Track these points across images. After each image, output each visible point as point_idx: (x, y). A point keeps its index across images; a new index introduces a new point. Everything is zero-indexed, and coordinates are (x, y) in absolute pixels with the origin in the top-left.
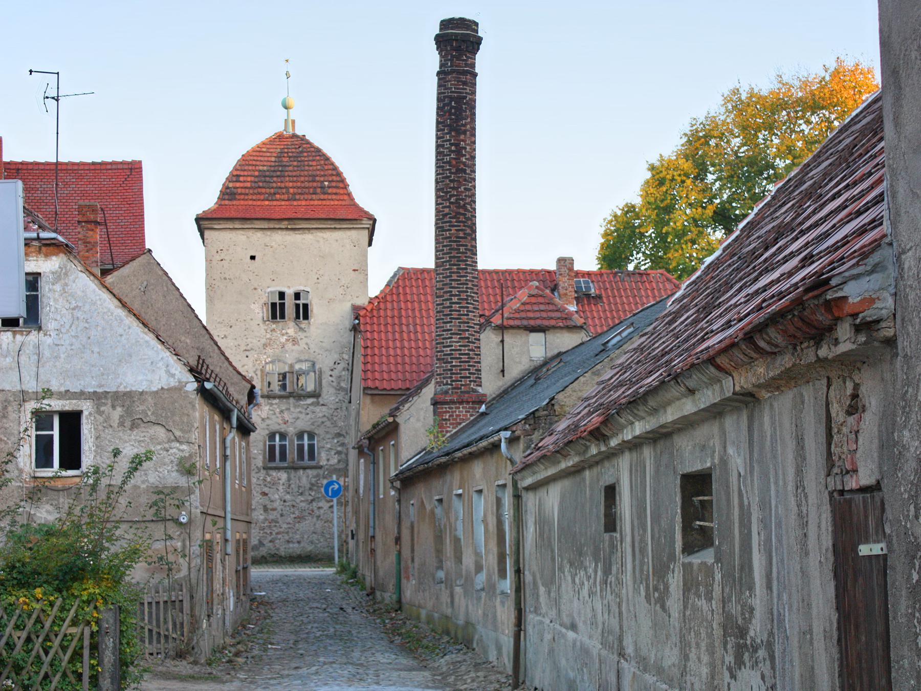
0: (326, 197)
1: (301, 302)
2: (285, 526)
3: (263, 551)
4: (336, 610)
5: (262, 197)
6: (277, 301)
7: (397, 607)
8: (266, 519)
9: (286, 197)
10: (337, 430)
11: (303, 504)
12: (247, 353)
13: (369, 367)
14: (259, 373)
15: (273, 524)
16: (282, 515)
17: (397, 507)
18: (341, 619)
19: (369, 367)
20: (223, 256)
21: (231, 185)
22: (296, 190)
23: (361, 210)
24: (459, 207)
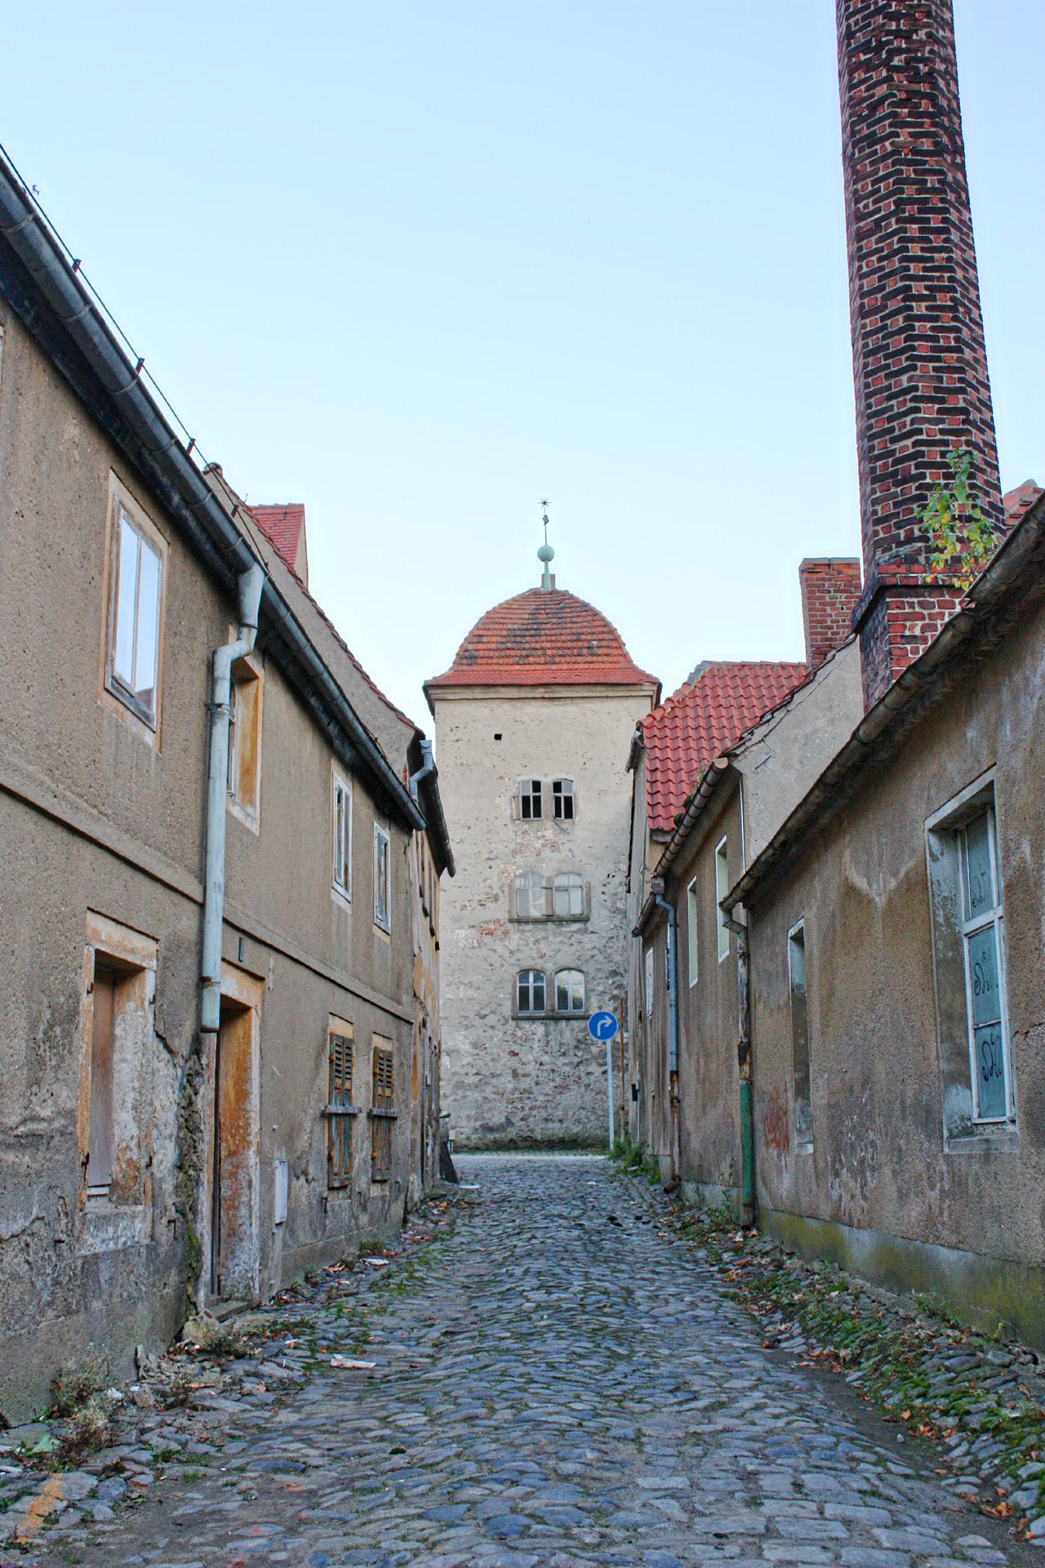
0: (594, 659)
1: (562, 795)
2: (541, 1098)
3: (512, 1133)
4: (599, 1222)
5: (511, 661)
6: (531, 794)
7: (745, 1218)
8: (516, 1089)
9: (542, 660)
10: (611, 967)
11: (567, 1069)
12: (491, 863)
13: (659, 798)
14: (506, 889)
15: (525, 1095)
16: (537, 1084)
17: (742, 970)
18: (607, 1245)
19: (659, 798)
20: (459, 735)
21: (470, 647)
22: (555, 652)
23: (642, 673)
24: (916, 78)
